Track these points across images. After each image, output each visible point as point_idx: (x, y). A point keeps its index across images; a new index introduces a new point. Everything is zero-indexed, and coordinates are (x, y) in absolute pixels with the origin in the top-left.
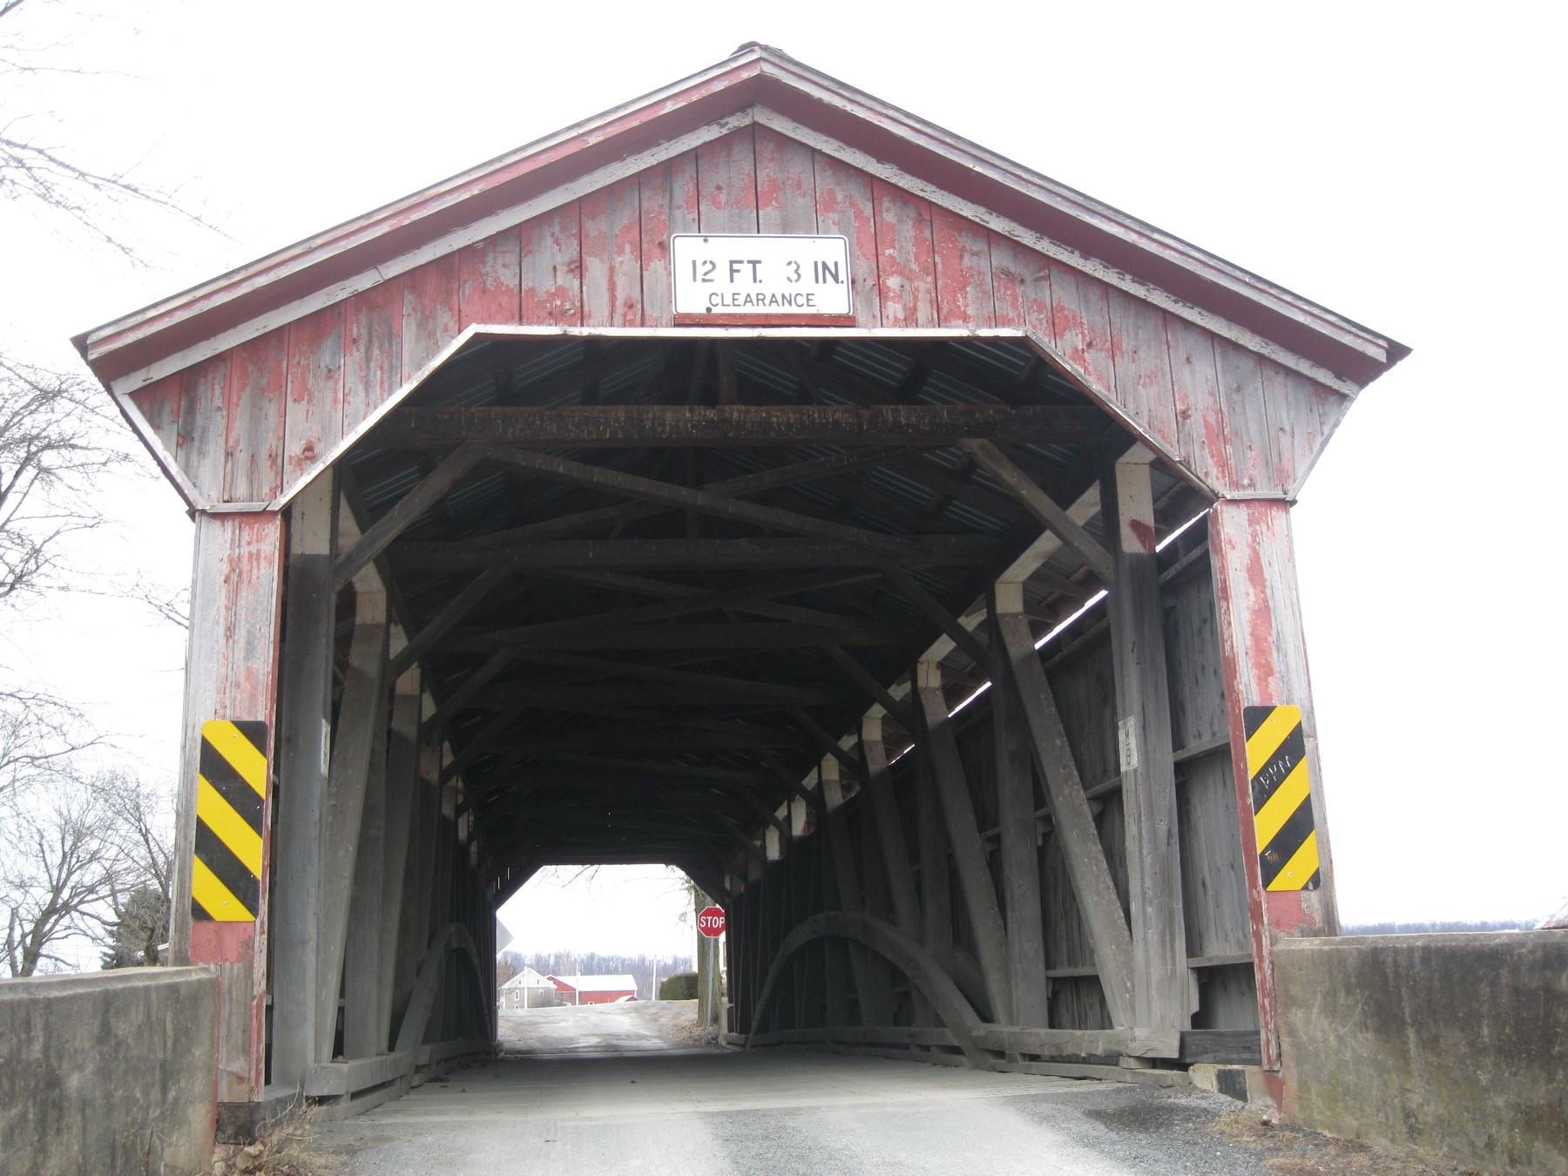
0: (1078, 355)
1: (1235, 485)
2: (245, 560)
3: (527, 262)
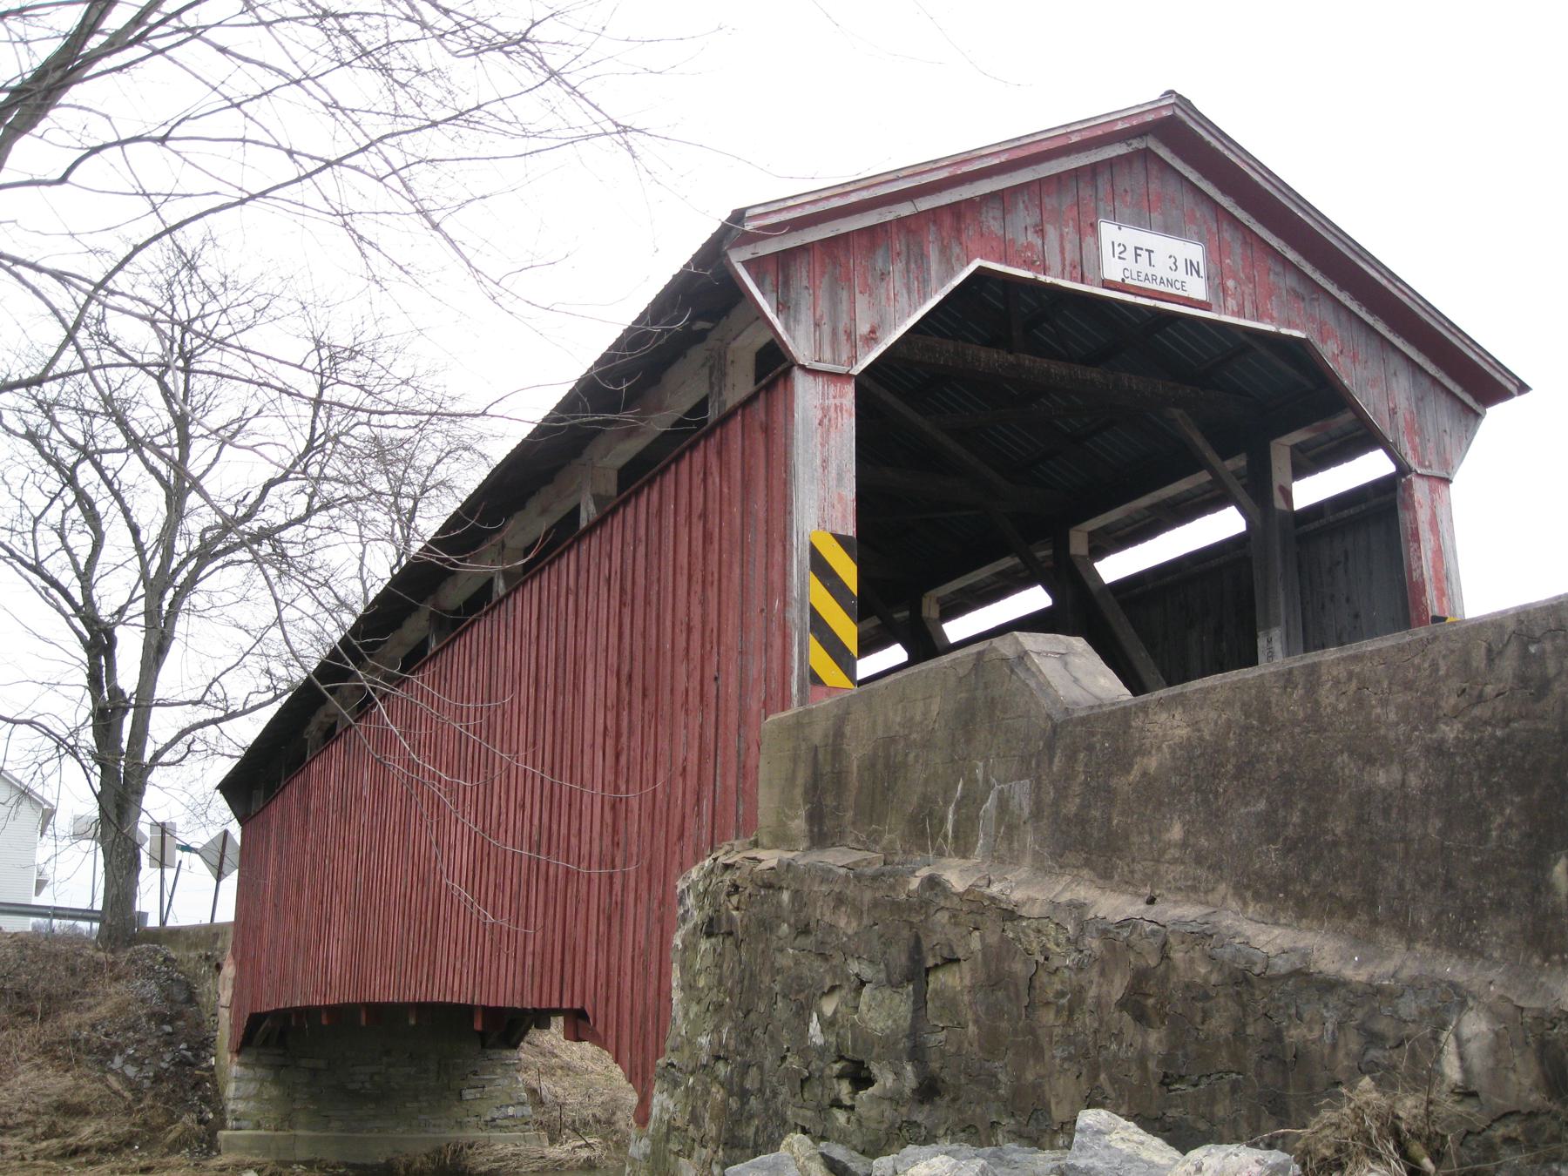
0: (1335, 358)
1: (1421, 464)
2: (832, 410)
3: (1008, 217)
